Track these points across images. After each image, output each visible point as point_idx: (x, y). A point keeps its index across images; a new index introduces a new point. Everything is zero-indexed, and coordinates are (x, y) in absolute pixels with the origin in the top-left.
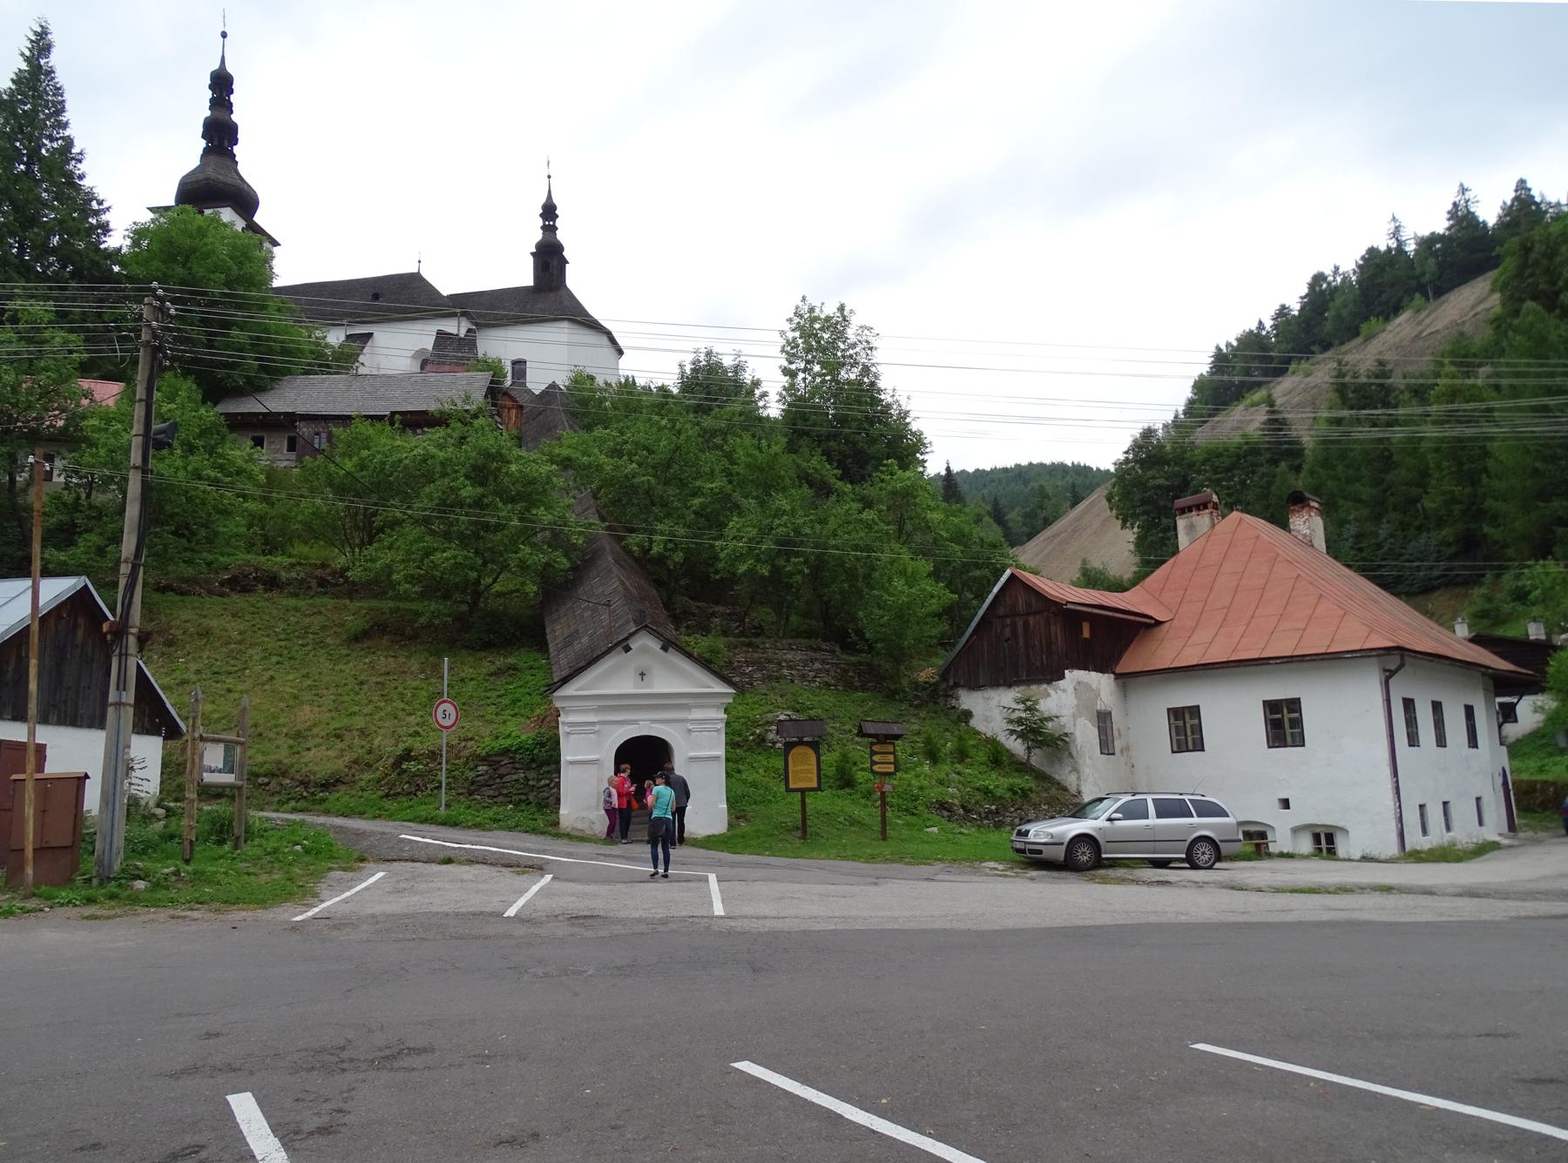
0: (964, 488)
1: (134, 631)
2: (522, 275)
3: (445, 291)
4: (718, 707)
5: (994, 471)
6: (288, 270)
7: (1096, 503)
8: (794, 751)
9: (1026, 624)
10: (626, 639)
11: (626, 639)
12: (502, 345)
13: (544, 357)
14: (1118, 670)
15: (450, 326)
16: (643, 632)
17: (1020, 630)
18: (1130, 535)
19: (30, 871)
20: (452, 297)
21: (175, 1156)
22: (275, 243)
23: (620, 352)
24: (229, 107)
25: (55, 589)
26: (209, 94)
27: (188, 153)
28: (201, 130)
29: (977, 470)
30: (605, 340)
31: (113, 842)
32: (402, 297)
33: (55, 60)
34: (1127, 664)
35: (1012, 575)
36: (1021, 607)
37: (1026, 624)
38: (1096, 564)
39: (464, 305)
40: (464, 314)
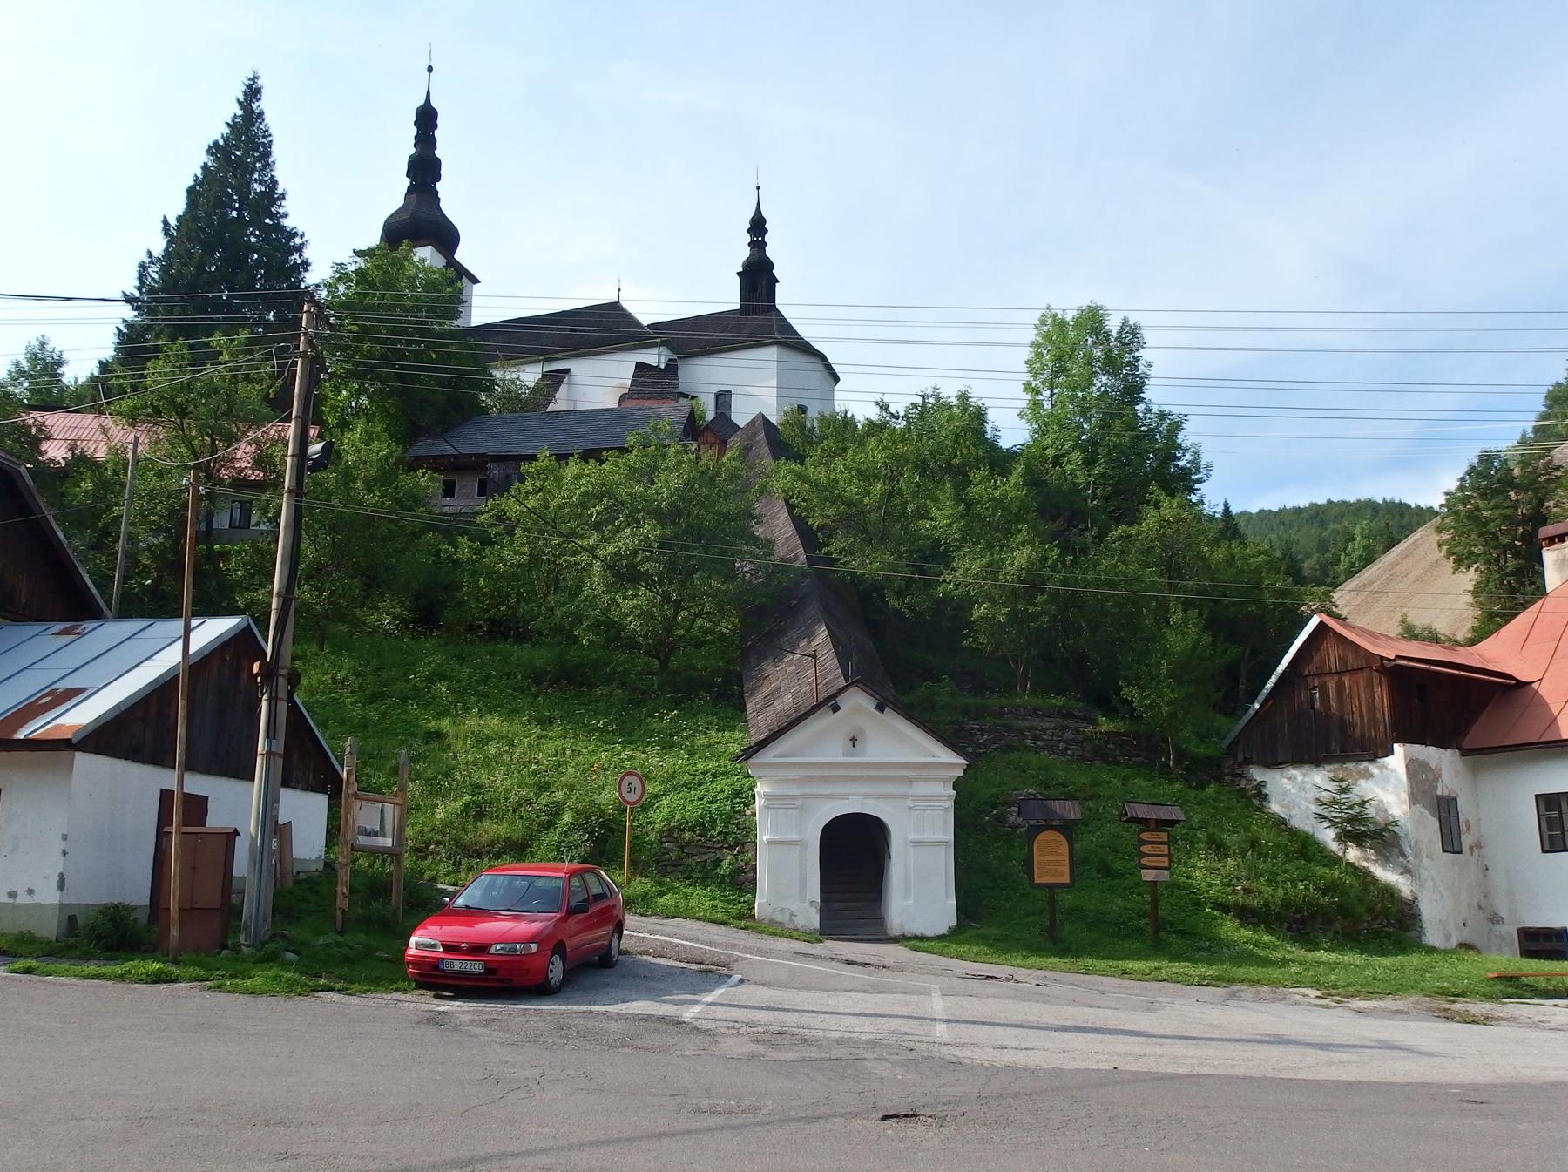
0: (1248, 531)
1: (283, 672)
2: (726, 296)
3: (645, 319)
4: (945, 781)
5: (1282, 511)
6: (486, 307)
7: (1425, 543)
8: (1041, 837)
9: (1340, 687)
10: (835, 696)
11: (835, 696)
12: (707, 376)
13: (753, 386)
14: (1466, 744)
15: (651, 357)
16: (854, 689)
17: (1332, 693)
18: (1469, 579)
19: (174, 932)
20: (652, 326)
21: (434, 1166)
22: (475, 281)
23: (836, 379)
24: (432, 143)
25: (210, 631)
26: (414, 131)
27: (393, 193)
28: (406, 168)
29: (1262, 511)
30: (819, 366)
31: (254, 904)
32: (602, 328)
33: (265, 104)
34: (1473, 738)
35: (1321, 623)
36: (1333, 664)
37: (1340, 687)
38: (1419, 621)
39: (665, 333)
40: (664, 344)
